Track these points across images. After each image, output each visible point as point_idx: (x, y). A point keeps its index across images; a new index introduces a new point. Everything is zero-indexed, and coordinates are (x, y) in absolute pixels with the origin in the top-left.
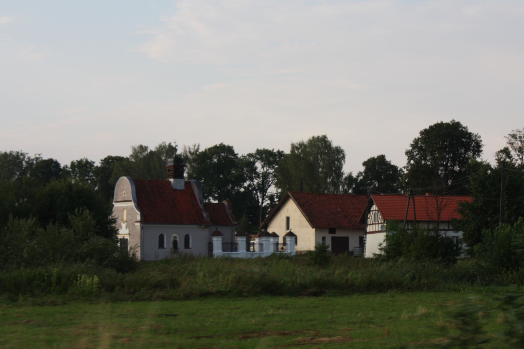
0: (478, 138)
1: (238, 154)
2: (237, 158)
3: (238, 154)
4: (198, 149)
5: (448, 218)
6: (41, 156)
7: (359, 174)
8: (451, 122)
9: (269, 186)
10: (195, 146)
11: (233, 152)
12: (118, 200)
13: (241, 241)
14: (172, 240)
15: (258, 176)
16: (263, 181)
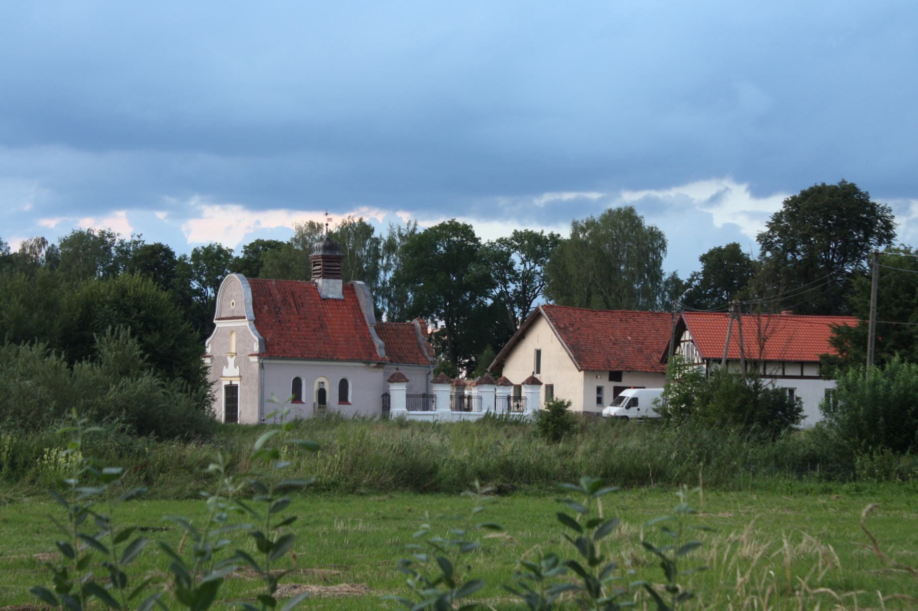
0: (887, 212)
1: (480, 238)
2: (479, 245)
3: (480, 238)
4: (415, 229)
5: (779, 355)
6: (142, 238)
7: (693, 276)
8: (840, 184)
9: (535, 296)
10: (409, 224)
11: (473, 235)
12: (223, 316)
13: (443, 393)
14: (316, 388)
15: (515, 277)
16: (524, 287)
